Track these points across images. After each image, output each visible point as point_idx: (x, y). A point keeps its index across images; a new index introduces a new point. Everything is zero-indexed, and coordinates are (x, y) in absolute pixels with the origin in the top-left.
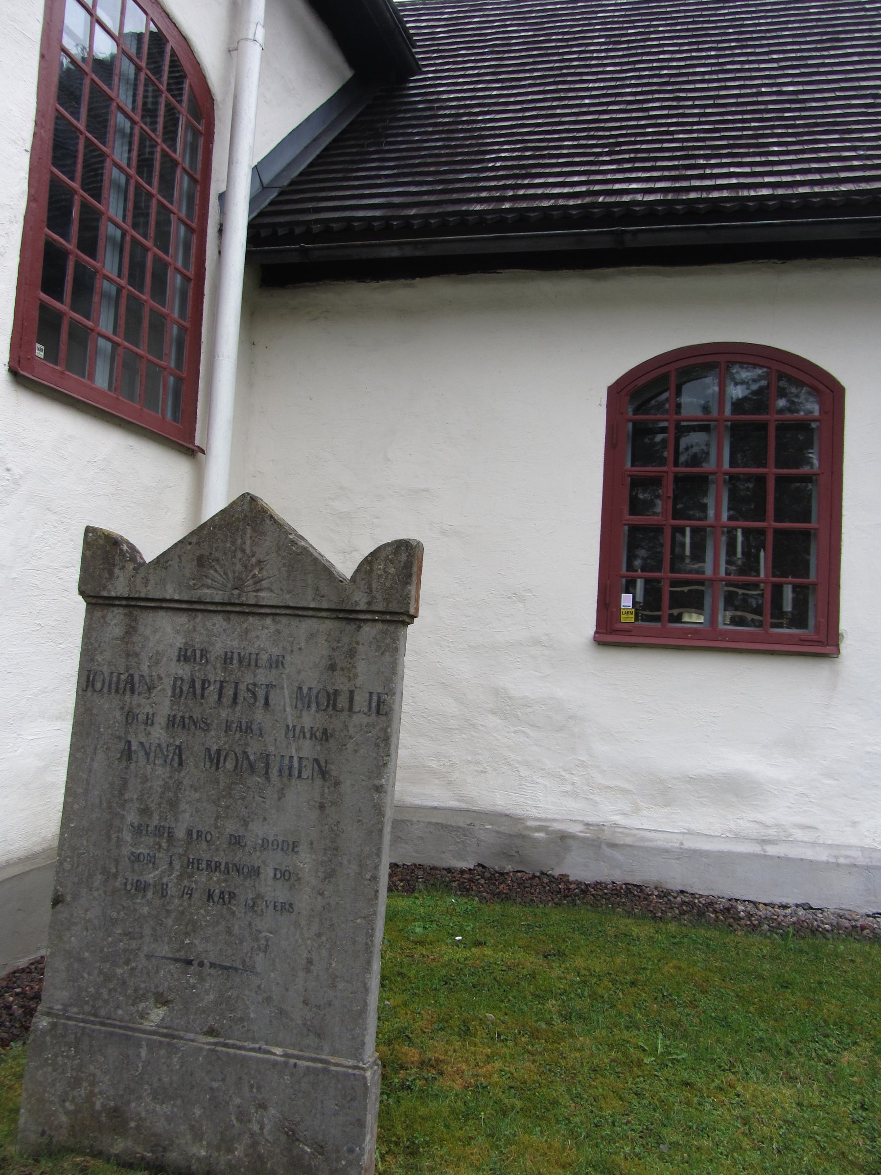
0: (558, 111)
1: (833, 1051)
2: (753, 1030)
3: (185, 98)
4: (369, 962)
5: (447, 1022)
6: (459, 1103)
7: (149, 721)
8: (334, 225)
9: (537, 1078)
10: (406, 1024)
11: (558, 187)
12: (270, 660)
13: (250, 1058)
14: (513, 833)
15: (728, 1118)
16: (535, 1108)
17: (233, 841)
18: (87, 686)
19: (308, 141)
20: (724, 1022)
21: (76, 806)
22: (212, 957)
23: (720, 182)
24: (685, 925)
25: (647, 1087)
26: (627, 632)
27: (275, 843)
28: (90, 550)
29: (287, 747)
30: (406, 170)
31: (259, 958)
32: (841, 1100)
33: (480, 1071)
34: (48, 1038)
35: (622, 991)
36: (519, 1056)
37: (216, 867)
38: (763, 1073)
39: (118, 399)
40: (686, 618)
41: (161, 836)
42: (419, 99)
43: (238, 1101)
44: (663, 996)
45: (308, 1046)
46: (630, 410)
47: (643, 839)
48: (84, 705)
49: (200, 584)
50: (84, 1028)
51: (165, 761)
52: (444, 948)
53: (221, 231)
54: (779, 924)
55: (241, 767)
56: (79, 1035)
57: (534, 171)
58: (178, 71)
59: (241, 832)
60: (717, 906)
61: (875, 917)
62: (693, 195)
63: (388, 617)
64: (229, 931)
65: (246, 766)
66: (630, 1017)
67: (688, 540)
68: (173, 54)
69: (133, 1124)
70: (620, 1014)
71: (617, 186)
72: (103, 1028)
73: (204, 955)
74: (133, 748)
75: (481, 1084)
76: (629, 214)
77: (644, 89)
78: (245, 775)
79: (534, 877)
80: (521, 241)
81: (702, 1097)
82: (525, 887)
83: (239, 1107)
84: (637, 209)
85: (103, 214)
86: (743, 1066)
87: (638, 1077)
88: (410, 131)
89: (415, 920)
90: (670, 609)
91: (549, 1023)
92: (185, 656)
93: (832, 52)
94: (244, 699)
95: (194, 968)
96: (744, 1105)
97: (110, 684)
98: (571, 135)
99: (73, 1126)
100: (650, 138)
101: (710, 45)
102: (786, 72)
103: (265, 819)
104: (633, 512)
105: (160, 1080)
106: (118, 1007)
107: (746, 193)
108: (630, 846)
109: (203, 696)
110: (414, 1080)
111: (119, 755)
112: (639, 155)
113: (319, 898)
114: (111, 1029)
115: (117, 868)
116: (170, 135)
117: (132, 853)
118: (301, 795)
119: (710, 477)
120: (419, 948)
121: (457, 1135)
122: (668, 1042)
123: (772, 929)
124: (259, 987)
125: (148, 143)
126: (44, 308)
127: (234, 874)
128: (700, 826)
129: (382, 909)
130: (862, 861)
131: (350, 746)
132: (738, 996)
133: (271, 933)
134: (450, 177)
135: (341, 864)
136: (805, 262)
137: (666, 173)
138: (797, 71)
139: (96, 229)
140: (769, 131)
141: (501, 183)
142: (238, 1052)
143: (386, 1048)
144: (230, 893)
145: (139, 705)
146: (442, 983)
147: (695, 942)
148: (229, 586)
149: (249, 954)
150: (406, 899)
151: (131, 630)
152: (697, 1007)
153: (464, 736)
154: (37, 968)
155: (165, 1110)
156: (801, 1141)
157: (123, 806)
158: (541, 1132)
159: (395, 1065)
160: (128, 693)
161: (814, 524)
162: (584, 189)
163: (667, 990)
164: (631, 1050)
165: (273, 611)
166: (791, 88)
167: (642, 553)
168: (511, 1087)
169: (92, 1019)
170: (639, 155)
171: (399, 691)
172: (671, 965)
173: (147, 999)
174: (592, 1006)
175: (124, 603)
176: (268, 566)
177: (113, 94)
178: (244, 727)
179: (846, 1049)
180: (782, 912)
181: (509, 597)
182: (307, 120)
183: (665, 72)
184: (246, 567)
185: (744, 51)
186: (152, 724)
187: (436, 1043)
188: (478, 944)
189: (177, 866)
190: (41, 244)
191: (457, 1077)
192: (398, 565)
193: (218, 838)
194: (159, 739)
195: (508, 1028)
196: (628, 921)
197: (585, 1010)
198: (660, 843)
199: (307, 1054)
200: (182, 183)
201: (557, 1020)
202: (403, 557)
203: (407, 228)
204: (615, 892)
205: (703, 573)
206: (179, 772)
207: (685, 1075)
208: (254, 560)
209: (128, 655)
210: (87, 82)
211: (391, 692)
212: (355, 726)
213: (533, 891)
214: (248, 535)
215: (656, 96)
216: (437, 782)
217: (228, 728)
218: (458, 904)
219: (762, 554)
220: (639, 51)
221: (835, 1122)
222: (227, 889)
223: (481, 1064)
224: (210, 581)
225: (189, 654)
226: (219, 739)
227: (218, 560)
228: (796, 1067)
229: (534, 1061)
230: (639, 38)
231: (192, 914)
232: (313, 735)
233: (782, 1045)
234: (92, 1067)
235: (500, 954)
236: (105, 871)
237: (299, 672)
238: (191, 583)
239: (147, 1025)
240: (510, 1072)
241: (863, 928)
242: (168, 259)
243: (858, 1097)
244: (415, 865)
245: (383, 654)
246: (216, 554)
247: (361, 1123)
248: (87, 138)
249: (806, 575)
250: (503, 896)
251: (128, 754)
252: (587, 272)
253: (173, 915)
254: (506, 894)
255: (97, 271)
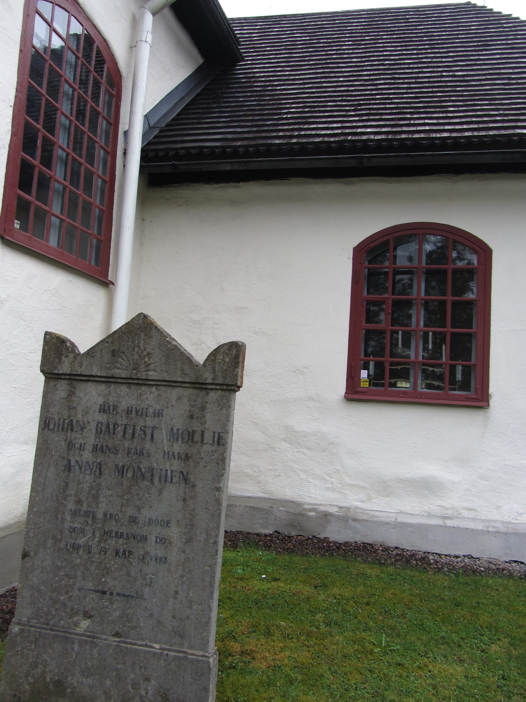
0: (324, 85)
1: (486, 644)
2: (438, 631)
3: (105, 74)
4: (212, 593)
5: (257, 627)
6: (265, 677)
7: (82, 448)
8: (192, 151)
9: (310, 661)
10: (233, 628)
11: (325, 130)
12: (154, 412)
13: (140, 650)
14: (296, 512)
15: (424, 685)
16: (309, 679)
17: (131, 520)
18: (45, 427)
19: (177, 100)
20: (421, 627)
21: (37, 499)
22: (118, 590)
23: (419, 128)
24: (398, 568)
25: (376, 666)
26: (364, 393)
27: (157, 521)
28: (47, 346)
29: (164, 464)
30: (235, 119)
31: (146, 590)
32: (491, 674)
33: (277, 657)
34: (18, 638)
35: (361, 608)
36: (300, 648)
37: (121, 535)
38: (444, 658)
39: (63, 253)
40: (399, 385)
41: (88, 517)
42: (242, 76)
43: (132, 676)
44: (386, 611)
45: (175, 643)
46: (367, 263)
47: (373, 516)
48: (43, 438)
49: (113, 367)
50: (40, 632)
51: (91, 472)
52: (255, 582)
53: (125, 153)
54: (454, 567)
55: (137, 475)
56: (37, 636)
57: (310, 120)
58: (100, 57)
59: (136, 514)
60: (417, 556)
61: (510, 563)
62: (403, 136)
63: (225, 387)
64: (128, 574)
65: (139, 475)
66: (366, 624)
67: (400, 336)
68: (98, 47)
69: (69, 690)
70: (360, 622)
71: (359, 130)
72: (52, 632)
73: (113, 588)
74: (72, 464)
75: (277, 665)
76: (366, 147)
77: (375, 72)
78: (139, 481)
79: (308, 539)
80: (302, 162)
81: (409, 672)
82: (303, 545)
83: (133, 680)
84: (371, 144)
85: (56, 143)
86: (432, 654)
87: (371, 660)
88: (237, 95)
89: (237, 565)
90: (390, 379)
91: (318, 628)
92: (104, 409)
93: (484, 53)
94: (139, 435)
95: (107, 596)
96: (433, 677)
97: (58, 426)
98: (332, 99)
99: (33, 692)
100: (378, 102)
101: (413, 47)
102: (458, 64)
103: (150, 507)
104: (367, 322)
105: (85, 663)
106: (61, 619)
107: (434, 135)
108: (366, 520)
109: (114, 434)
110: (238, 662)
111: (63, 468)
112: (372, 112)
113: (183, 554)
114: (57, 633)
115: (61, 536)
116: (96, 97)
117: (71, 527)
118: (172, 493)
119: (414, 301)
120: (240, 582)
121: (263, 696)
122: (388, 639)
123: (449, 570)
124: (146, 607)
125: (82, 100)
126: (20, 198)
127: (132, 540)
128: (407, 508)
129: (220, 561)
130: (502, 529)
131: (202, 464)
132: (430, 611)
133: (153, 575)
134: (261, 123)
135: (196, 534)
136: (468, 175)
137: (388, 123)
138: (464, 63)
139: (52, 151)
140: (448, 99)
141: (291, 127)
142: (133, 647)
143: (220, 643)
144: (129, 551)
145: (76, 438)
146: (254, 604)
147: (404, 578)
148: (131, 368)
149: (140, 588)
150: (232, 553)
151: (71, 394)
152: (405, 618)
153: (268, 454)
154: (13, 593)
155: (89, 682)
156: (467, 699)
157: (65, 499)
158: (313, 694)
159: (226, 654)
160: (69, 431)
161: (474, 330)
162: (339, 131)
163: (388, 608)
164: (367, 644)
165: (157, 383)
166: (460, 73)
167: (373, 343)
168: (295, 667)
169: (45, 626)
170: (372, 112)
171: (231, 431)
172: (390, 592)
173: (78, 615)
174: (343, 617)
175: (68, 377)
176: (154, 356)
177: (62, 73)
178: (138, 452)
179: (493, 643)
180: (455, 560)
181: (294, 372)
182: (176, 88)
183: (387, 62)
184: (140, 357)
185: (433, 51)
186: (84, 450)
187: (250, 640)
188: (275, 580)
189: (98, 534)
190: (19, 162)
191: (263, 661)
192: (231, 357)
193: (122, 518)
194: (88, 458)
195: (293, 631)
196: (365, 566)
197: (339, 620)
198: (383, 519)
199: (174, 648)
200: (102, 124)
201: (322, 626)
202: (234, 352)
203: (235, 153)
204: (356, 548)
205: (409, 358)
206: (100, 479)
207: (399, 659)
208: (145, 353)
209: (69, 408)
210: (47, 65)
211: (226, 432)
212: (205, 452)
213: (308, 547)
214: (142, 338)
215: (382, 77)
216: (251, 481)
217: (129, 453)
218: (263, 556)
219: (444, 347)
220: (372, 50)
221: (487, 687)
222: (128, 549)
223: (277, 653)
224: (119, 365)
225: (106, 408)
226: (123, 459)
227: (124, 352)
228: (464, 654)
229: (309, 651)
230: (372, 42)
231: (106, 563)
232: (179, 457)
233: (455, 641)
234: (45, 656)
235: (289, 586)
236: (54, 537)
237: (171, 420)
238: (108, 366)
239: (78, 630)
240: (295, 658)
241: (503, 570)
242: (94, 170)
243: (501, 672)
244: (237, 531)
245: (221, 409)
246: (123, 349)
247: (206, 690)
248: (47, 100)
249: (470, 360)
250: (290, 550)
251: (69, 468)
252: (341, 180)
253: (95, 564)
254: (292, 549)
255: (51, 177)
